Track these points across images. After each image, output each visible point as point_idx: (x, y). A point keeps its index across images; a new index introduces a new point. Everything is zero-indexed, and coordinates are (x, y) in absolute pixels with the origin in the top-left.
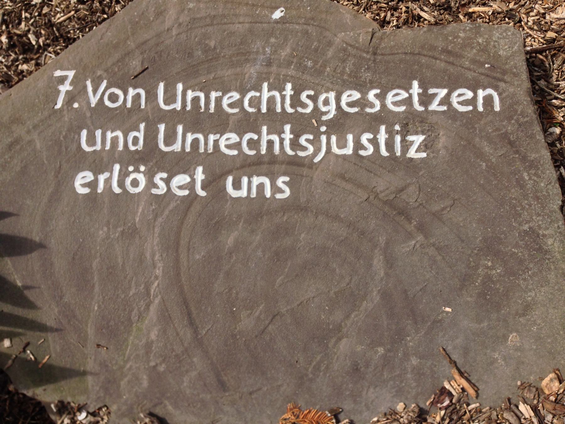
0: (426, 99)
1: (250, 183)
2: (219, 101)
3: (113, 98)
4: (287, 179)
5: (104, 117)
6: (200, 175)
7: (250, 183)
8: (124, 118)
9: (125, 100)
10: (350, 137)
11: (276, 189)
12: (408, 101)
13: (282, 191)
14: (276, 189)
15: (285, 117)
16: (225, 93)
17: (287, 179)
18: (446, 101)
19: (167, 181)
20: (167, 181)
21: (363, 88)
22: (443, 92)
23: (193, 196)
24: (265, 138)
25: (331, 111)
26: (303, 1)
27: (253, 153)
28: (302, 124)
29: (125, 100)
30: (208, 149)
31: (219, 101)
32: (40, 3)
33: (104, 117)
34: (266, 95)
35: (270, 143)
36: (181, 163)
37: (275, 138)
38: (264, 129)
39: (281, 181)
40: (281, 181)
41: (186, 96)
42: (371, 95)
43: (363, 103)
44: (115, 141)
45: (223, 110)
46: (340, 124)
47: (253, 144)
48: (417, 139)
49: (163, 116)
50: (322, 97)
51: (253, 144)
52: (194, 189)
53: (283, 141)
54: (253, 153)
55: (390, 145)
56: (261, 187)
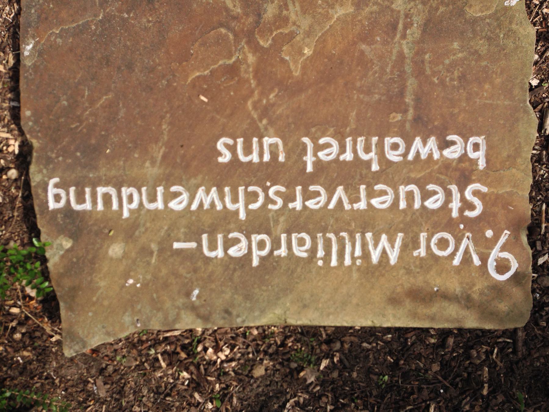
1: (261, 155)
2: (343, 150)
3: (443, 244)
4: (220, 160)
7: (261, 155)
9: (428, 240)
11: (232, 149)
13: (227, 146)
14: (232, 149)
17: (220, 160)
19: (268, 200)
20: (268, 200)
24: (241, 205)
27: (251, 189)
29: (428, 240)
30: (351, 142)
31: (343, 150)
32: (525, 328)
35: (235, 200)
38: (242, 215)
39: (226, 157)
40: (226, 157)
45: (327, 189)
52: (311, 238)
54: (251, 189)
56: (248, 150)
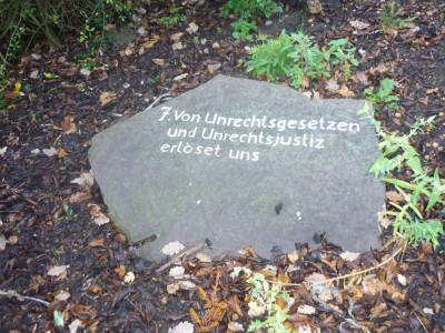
0: (326, 125)
5: (179, 123)
6: (218, 148)
8: (188, 126)
10: (290, 138)
12: (318, 125)
15: (261, 129)
16: (244, 119)
18: (335, 126)
21: (298, 120)
22: (334, 123)
23: (213, 156)
25: (283, 128)
26: (408, 2)
28: (267, 131)
33: (179, 123)
34: (254, 120)
35: (256, 123)
36: (213, 143)
37: (258, 120)
41: (219, 119)
42: (302, 122)
43: (297, 126)
44: (222, 121)
46: (287, 133)
47: (248, 123)
48: (321, 141)
49: (206, 125)
50: (280, 122)
51: (248, 123)
53: (258, 139)
55: (308, 141)
